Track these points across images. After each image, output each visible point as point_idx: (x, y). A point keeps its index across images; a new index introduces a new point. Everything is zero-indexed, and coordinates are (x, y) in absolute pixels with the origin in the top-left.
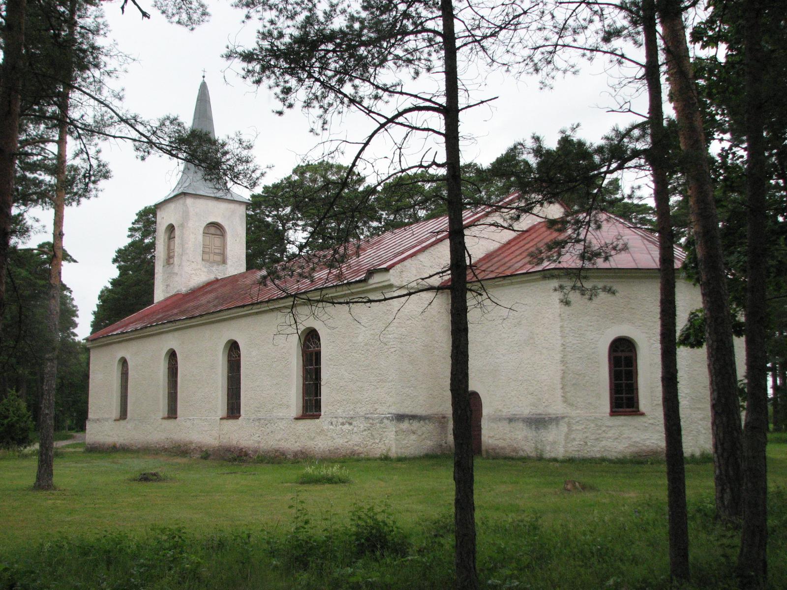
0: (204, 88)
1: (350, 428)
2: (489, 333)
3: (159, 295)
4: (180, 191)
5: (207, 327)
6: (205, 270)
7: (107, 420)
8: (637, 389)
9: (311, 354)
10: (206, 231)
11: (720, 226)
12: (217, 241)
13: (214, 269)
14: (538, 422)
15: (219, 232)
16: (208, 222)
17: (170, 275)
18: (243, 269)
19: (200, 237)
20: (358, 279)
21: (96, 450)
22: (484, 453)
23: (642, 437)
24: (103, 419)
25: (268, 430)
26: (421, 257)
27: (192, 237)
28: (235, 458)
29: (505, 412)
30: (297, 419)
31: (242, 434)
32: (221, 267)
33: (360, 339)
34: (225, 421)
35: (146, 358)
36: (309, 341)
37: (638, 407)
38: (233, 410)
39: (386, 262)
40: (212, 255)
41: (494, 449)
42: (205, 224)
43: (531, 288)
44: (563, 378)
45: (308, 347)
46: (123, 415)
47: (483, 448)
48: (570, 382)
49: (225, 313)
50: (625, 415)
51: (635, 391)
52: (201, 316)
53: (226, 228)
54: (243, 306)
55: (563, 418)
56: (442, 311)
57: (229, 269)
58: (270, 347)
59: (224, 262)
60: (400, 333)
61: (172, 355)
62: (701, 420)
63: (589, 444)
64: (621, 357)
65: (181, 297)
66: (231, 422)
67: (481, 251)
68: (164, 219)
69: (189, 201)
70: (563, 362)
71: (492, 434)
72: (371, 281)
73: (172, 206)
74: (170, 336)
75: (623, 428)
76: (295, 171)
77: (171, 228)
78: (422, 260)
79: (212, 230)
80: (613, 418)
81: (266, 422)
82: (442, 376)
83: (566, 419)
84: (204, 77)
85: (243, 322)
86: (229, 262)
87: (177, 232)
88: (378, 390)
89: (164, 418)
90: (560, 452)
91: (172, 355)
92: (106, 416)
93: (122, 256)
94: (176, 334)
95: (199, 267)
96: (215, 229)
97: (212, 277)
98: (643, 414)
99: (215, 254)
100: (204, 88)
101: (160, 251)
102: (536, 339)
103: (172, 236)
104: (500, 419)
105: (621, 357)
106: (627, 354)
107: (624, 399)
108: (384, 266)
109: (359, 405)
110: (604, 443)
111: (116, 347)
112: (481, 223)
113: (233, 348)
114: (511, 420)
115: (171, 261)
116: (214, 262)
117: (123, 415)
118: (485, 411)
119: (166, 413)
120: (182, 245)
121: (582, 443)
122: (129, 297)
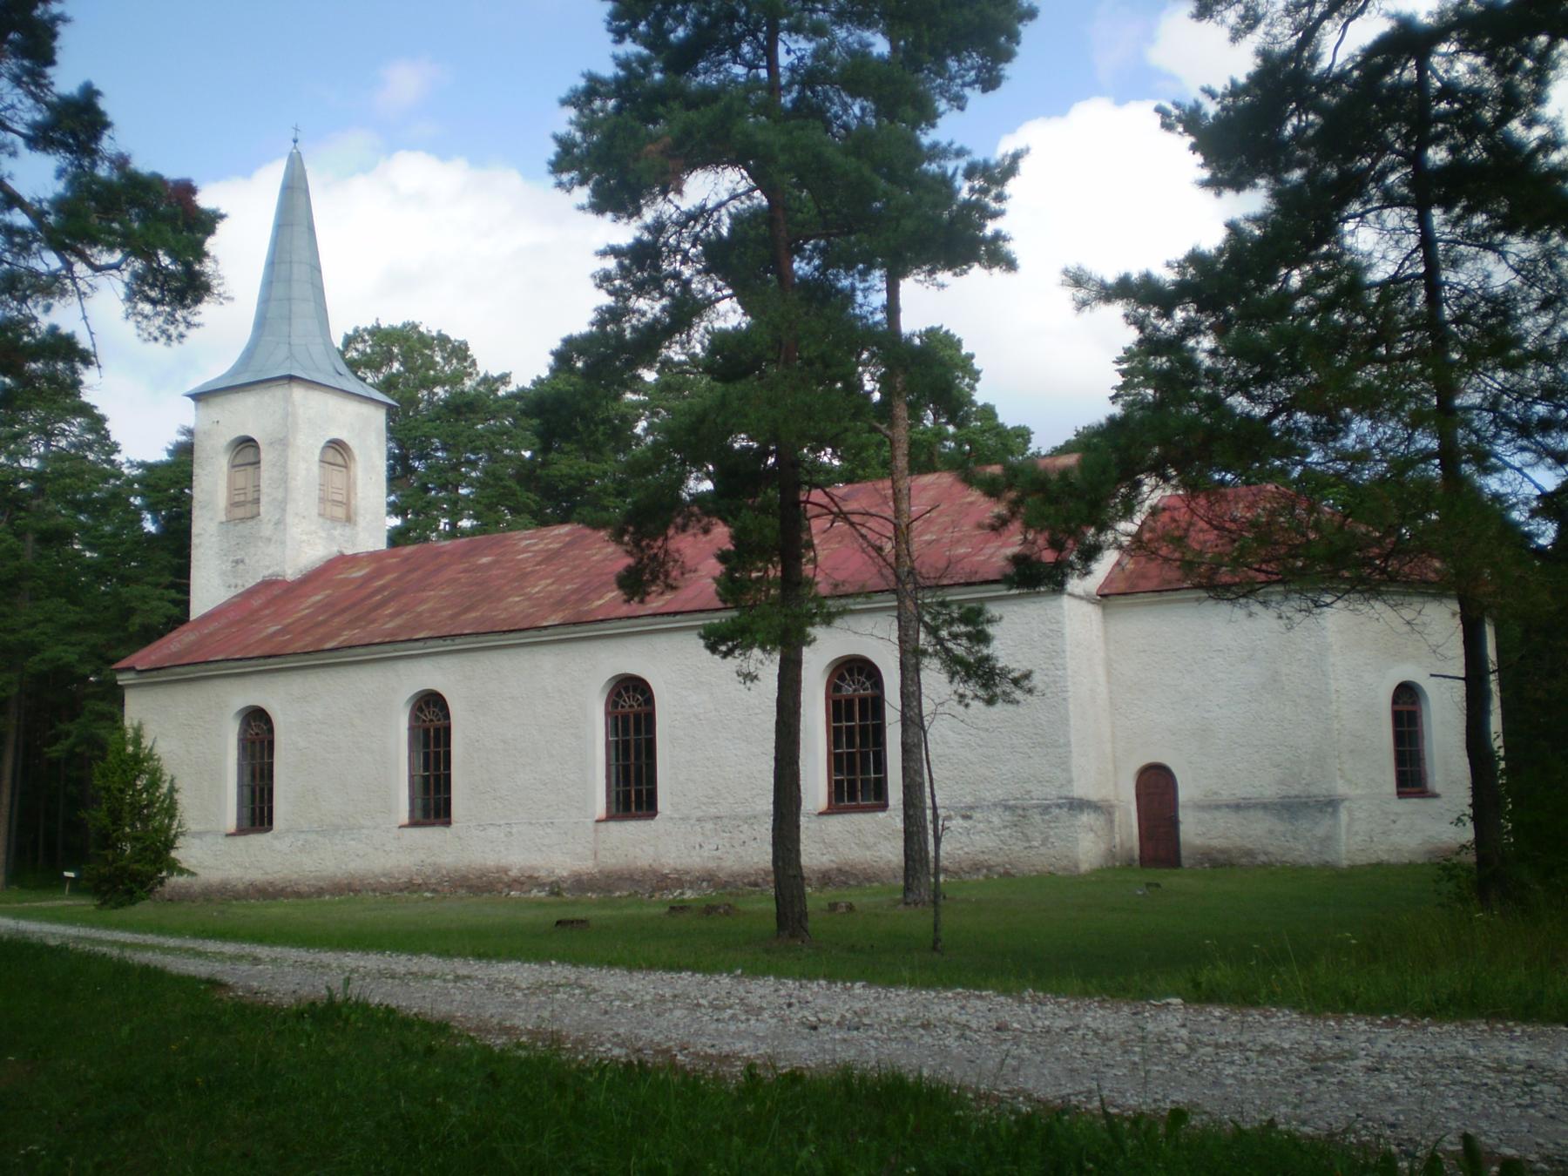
1: (967, 824)
6: (323, 534)
13: (336, 533)
15: (339, 460)
19: (315, 469)
22: (1186, 862)
29: (1226, 795)
30: (821, 814)
34: (603, 825)
37: (1425, 785)
41: (1222, 851)
42: (322, 444)
47: (1184, 853)
53: (356, 452)
59: (349, 519)
65: (276, 591)
69: (298, 393)
71: (1193, 830)
74: (426, 664)
79: (332, 455)
80: (1403, 801)
86: (362, 522)
97: (333, 550)
98: (1435, 796)
104: (1218, 807)
106: (1410, 708)
107: (1410, 775)
114: (1237, 807)
118: (1184, 794)
120: (284, 481)
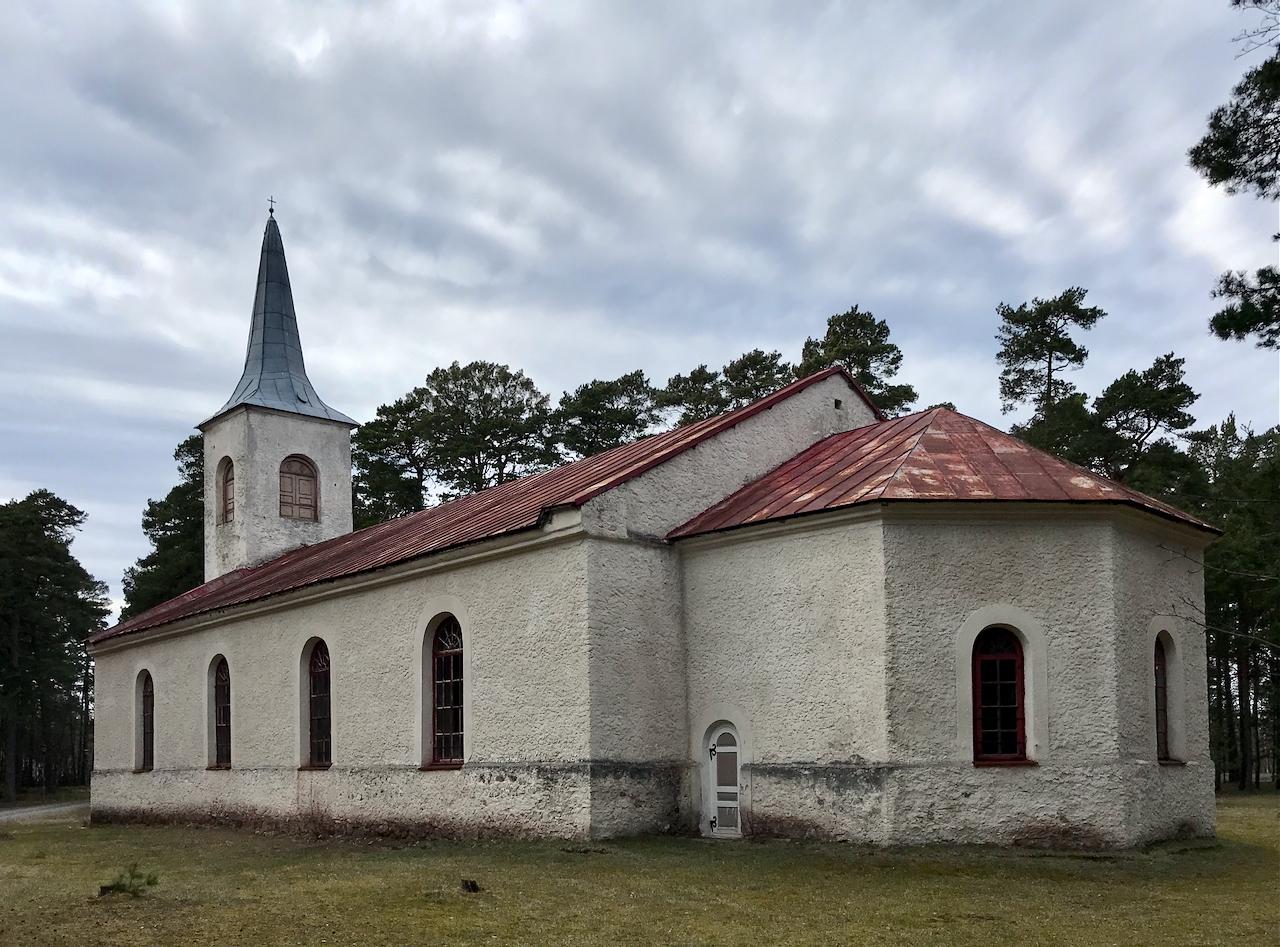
0: (272, 226)
2: (754, 620)
3: (213, 571)
4: (241, 401)
5: (276, 618)
7: (123, 771)
8: (1023, 719)
9: (447, 657)
10: (285, 469)
11: (1126, 466)
12: (304, 486)
14: (844, 775)
15: (306, 471)
16: (288, 454)
17: (227, 538)
18: (349, 529)
19: (276, 479)
20: (524, 524)
21: (105, 819)
23: (1033, 804)
24: (116, 771)
25: (376, 788)
26: (636, 486)
27: (261, 480)
28: (319, 834)
31: (337, 795)
32: (311, 528)
33: (530, 629)
35: (180, 671)
36: (444, 638)
38: (319, 755)
39: (573, 493)
40: (296, 508)
43: (833, 537)
44: (890, 699)
45: (443, 647)
46: (146, 764)
48: (904, 706)
49: (304, 592)
50: (1001, 766)
51: (1019, 723)
52: (263, 598)
53: (319, 464)
54: (331, 580)
55: (891, 770)
56: (671, 582)
57: (326, 531)
58: (377, 646)
59: (316, 519)
60: (600, 618)
61: (220, 666)
62: (1137, 776)
63: (936, 817)
64: (994, 662)
66: (317, 776)
67: (737, 479)
68: (217, 447)
70: (891, 669)
72: (549, 528)
73: (227, 427)
75: (998, 789)
76: (430, 379)
77: (227, 464)
78: (636, 490)
79: (296, 467)
81: (373, 775)
82: (669, 695)
83: (896, 773)
84: (271, 211)
85: (333, 607)
87: (237, 470)
88: (560, 720)
89: (209, 769)
90: (883, 831)
91: (220, 666)
92: (122, 766)
93: (156, 515)
94: (227, 630)
95: (275, 526)
96: (299, 467)
97: (297, 543)
99: (302, 506)
100: (272, 226)
101: (211, 499)
102: (841, 629)
103: (230, 476)
105: (994, 662)
108: (571, 499)
109: (527, 746)
110: (962, 817)
111: (132, 653)
112: (736, 521)
113: (317, 653)
115: (230, 517)
116: (301, 519)
117: (146, 764)
119: (215, 760)
121: (923, 814)
122: (171, 582)
